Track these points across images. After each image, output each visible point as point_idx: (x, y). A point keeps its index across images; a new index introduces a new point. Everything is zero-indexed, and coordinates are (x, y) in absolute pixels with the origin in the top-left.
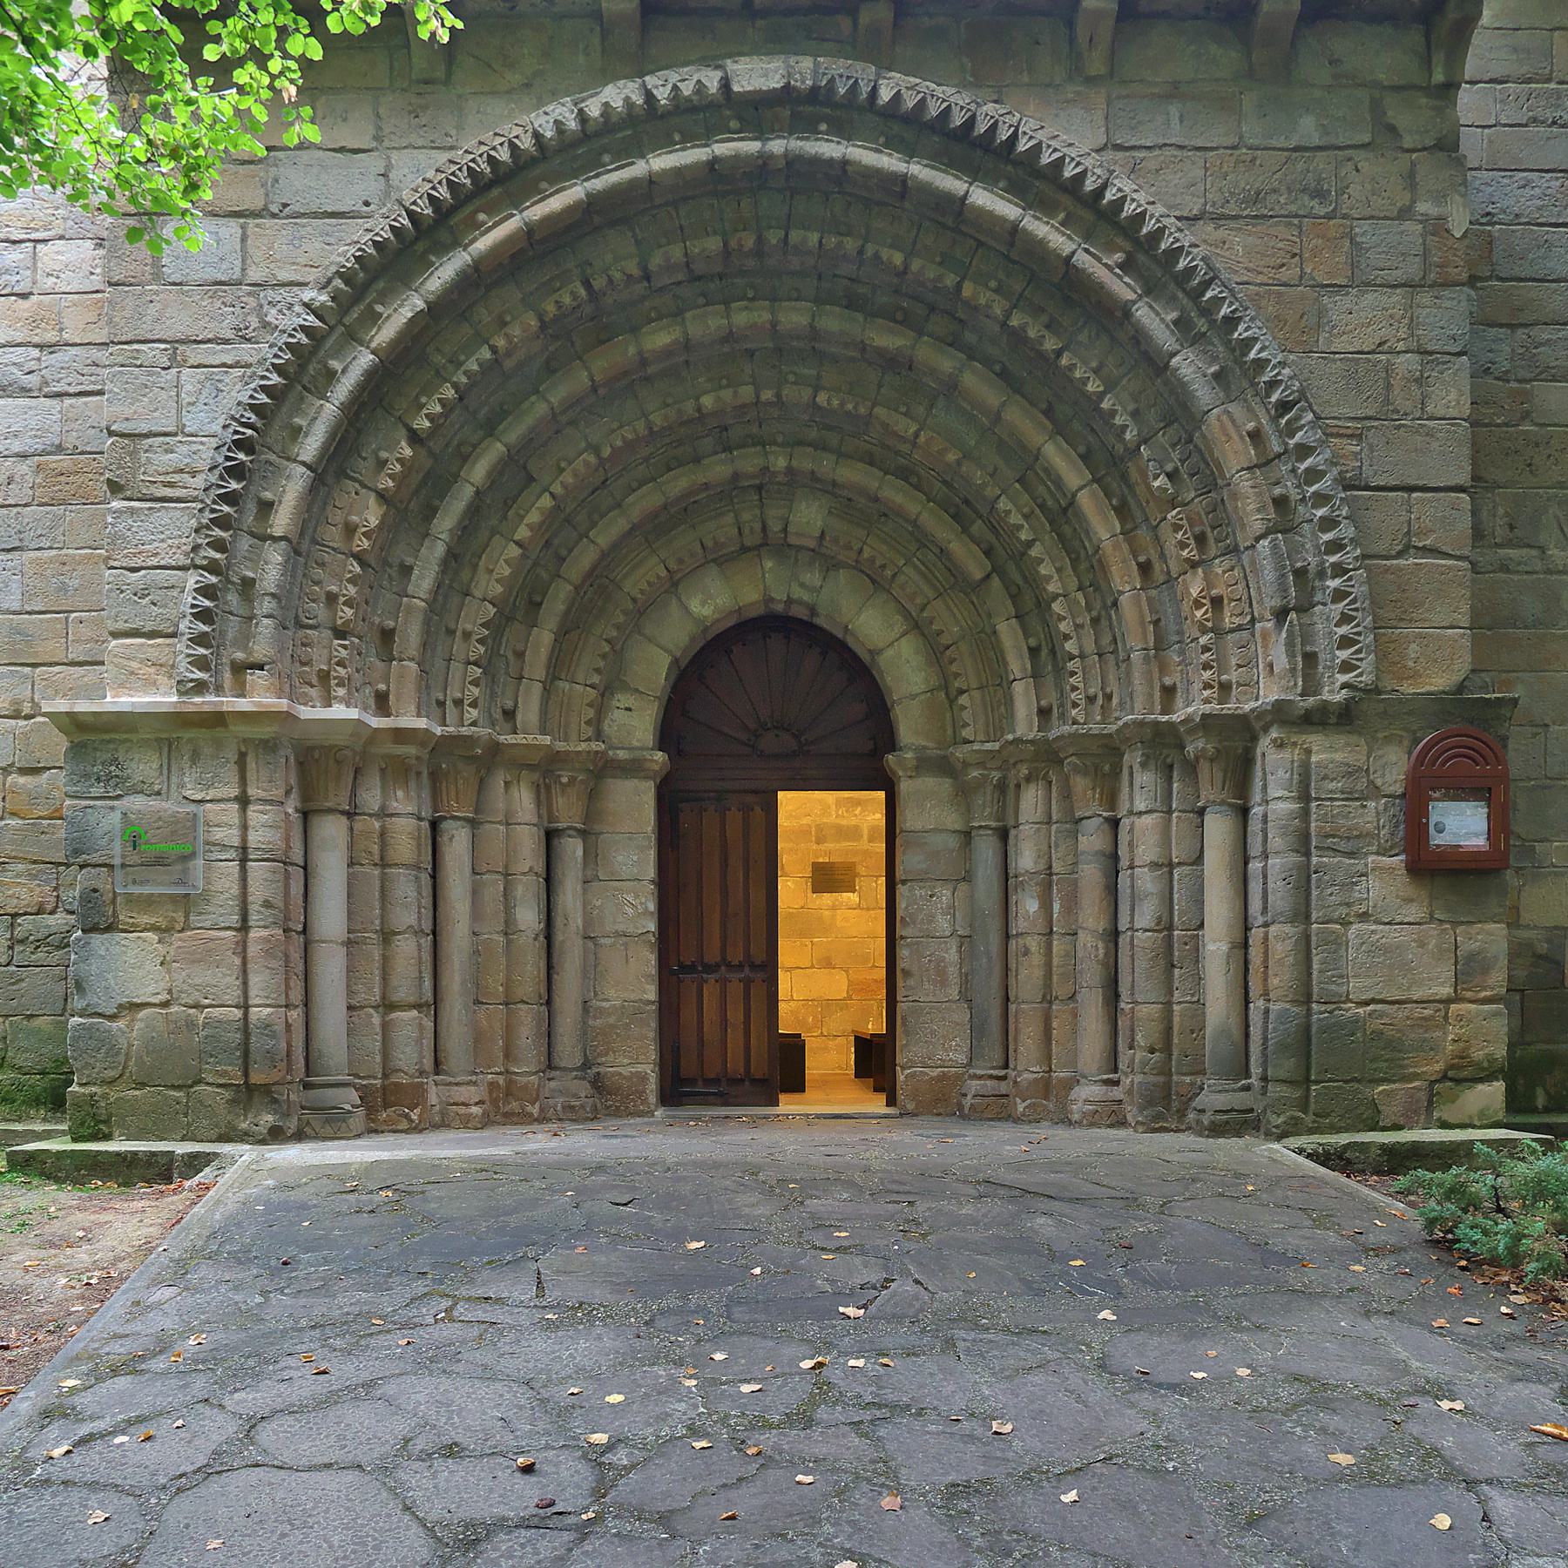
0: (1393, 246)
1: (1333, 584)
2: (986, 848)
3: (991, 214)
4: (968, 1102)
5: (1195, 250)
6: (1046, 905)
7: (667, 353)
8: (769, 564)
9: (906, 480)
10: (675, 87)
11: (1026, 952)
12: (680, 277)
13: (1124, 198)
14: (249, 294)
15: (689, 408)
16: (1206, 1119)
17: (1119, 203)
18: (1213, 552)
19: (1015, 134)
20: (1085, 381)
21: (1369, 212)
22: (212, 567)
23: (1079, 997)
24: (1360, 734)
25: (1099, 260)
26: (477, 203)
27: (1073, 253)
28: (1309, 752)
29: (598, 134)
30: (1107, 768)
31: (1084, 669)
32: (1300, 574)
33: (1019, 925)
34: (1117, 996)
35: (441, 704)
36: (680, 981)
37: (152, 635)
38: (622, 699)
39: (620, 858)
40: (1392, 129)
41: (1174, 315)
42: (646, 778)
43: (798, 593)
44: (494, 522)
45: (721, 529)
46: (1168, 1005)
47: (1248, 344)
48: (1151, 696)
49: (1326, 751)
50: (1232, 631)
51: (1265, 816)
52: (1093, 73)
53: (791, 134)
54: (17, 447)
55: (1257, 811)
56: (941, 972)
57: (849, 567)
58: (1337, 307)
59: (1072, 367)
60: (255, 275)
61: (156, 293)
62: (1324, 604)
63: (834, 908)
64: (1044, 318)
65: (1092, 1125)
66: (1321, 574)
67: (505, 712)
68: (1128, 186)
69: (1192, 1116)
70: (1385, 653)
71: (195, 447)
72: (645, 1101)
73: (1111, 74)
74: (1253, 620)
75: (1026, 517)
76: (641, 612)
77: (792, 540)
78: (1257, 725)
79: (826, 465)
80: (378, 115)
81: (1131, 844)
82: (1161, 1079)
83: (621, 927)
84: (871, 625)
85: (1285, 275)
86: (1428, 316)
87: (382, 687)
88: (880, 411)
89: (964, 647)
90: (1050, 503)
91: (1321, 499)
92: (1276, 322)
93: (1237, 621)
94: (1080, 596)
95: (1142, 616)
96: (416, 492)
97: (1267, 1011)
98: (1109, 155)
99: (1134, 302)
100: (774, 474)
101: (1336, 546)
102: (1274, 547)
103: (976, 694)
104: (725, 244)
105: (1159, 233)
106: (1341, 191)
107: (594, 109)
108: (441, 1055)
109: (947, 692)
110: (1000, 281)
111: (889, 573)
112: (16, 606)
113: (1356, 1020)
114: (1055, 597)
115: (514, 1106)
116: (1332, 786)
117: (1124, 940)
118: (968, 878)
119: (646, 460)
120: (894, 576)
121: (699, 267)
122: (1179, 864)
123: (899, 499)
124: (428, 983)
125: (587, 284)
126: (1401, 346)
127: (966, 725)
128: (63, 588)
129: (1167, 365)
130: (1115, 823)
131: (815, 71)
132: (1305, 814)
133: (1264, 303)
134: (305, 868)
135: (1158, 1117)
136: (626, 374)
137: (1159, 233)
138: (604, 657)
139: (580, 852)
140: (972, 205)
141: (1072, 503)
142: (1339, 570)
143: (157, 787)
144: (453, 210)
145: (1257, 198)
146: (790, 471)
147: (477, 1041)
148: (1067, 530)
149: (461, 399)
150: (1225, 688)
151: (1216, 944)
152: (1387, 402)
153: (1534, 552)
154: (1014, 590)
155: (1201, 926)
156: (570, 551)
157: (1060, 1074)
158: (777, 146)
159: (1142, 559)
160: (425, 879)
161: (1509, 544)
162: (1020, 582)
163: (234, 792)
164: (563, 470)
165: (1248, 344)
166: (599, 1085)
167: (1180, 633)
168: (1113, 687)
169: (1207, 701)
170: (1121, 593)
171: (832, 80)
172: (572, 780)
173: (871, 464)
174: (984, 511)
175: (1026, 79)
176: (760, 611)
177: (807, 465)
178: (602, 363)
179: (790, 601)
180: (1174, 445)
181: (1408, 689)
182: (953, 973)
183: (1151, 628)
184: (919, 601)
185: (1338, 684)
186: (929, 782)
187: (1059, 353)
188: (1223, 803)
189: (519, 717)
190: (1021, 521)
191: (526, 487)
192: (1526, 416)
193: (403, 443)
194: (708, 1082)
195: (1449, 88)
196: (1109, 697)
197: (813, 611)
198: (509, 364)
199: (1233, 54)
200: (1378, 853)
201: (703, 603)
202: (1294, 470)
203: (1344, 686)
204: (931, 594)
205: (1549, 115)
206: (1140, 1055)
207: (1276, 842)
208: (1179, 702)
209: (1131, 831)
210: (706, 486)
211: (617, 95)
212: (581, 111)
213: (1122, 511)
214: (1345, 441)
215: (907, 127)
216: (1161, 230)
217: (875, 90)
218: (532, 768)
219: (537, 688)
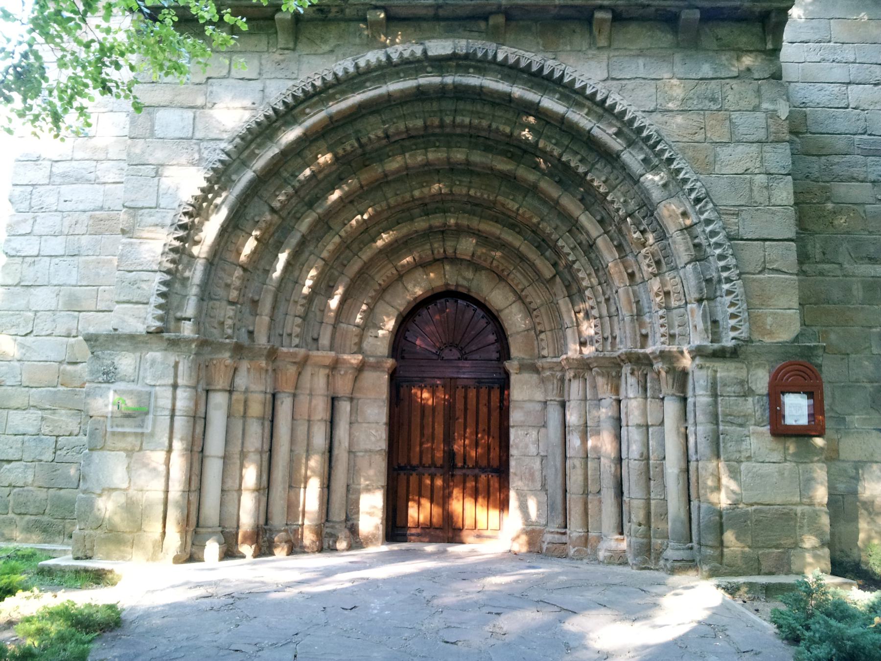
0: (751, 124)
1: (726, 287)
3: (551, 111)
4: (545, 546)
5: (652, 127)
7: (398, 171)
8: (447, 268)
9: (514, 230)
10: (401, 53)
11: (574, 467)
12: (404, 136)
13: (616, 103)
14: (195, 144)
15: (407, 196)
17: (613, 106)
19: (563, 74)
20: (599, 187)
21: (737, 108)
23: (602, 493)
24: (743, 363)
25: (605, 131)
26: (306, 104)
27: (592, 129)
28: (716, 371)
29: (365, 73)
30: (614, 374)
31: (602, 324)
32: (709, 281)
34: (622, 493)
36: (398, 474)
37: (137, 303)
39: (369, 411)
41: (642, 157)
42: (383, 371)
43: (462, 282)
44: (311, 248)
46: (648, 500)
47: (678, 171)
48: (635, 339)
49: (725, 371)
50: (676, 308)
51: (695, 404)
52: (601, 45)
53: (456, 73)
54: (81, 207)
55: (690, 400)
56: (532, 475)
57: (487, 269)
58: (724, 153)
59: (592, 180)
60: (198, 135)
61: (151, 142)
62: (722, 296)
64: (579, 157)
65: (609, 563)
66: (719, 281)
70: (752, 320)
71: (164, 214)
73: (610, 46)
74: (686, 303)
75: (572, 249)
77: (458, 256)
79: (475, 223)
80: (261, 64)
81: (626, 413)
82: (645, 540)
83: (368, 447)
84: (498, 298)
85: (697, 137)
86: (770, 156)
87: (251, 328)
88: (499, 198)
89: (543, 310)
91: (718, 245)
92: (693, 161)
93: (678, 303)
94: (599, 288)
96: (273, 234)
97: (699, 507)
98: (609, 83)
99: (622, 151)
100: (450, 226)
101: (726, 268)
102: (695, 269)
103: (549, 333)
104: (425, 123)
105: (633, 119)
106: (724, 99)
107: (362, 63)
108: (270, 516)
109: (536, 331)
110: (557, 140)
111: (506, 273)
112: (74, 283)
113: (746, 513)
114: (587, 288)
116: (728, 389)
117: (624, 463)
119: (387, 219)
120: (508, 275)
121: (413, 133)
122: (652, 425)
124: (265, 477)
125: (358, 140)
126: (757, 171)
127: (543, 349)
128: (98, 274)
129: (639, 180)
130: (619, 401)
131: (467, 46)
132: (716, 403)
133: (687, 151)
134: (205, 418)
135: (645, 562)
136: (377, 180)
137: (633, 119)
139: (348, 409)
140: (543, 108)
141: (594, 243)
142: (728, 280)
143: (132, 378)
144: (294, 107)
146: (457, 224)
147: (289, 507)
148: (593, 256)
149: (296, 192)
150: (672, 336)
151: (672, 467)
152: (751, 197)
153: (836, 266)
154: (567, 283)
155: (664, 458)
156: (349, 262)
157: (592, 534)
158: (449, 80)
159: (630, 271)
160: (267, 424)
161: (823, 262)
162: (569, 278)
163: (171, 381)
164: (345, 225)
165: (678, 171)
167: (650, 308)
168: (617, 332)
169: (663, 343)
170: (619, 288)
171: (475, 50)
172: (346, 373)
173: (496, 222)
175: (568, 48)
176: (444, 289)
177: (465, 222)
178: (366, 176)
179: (457, 285)
180: (644, 218)
181: (767, 340)
182: (538, 475)
183: (634, 305)
184: (520, 287)
185: (730, 337)
186: (526, 376)
187: (586, 174)
188: (673, 395)
189: (320, 342)
190: (569, 251)
191: (328, 232)
192: (828, 199)
193: (267, 213)
195: (776, 50)
196: (614, 338)
197: (469, 290)
198: (320, 176)
200: (755, 425)
202: (704, 231)
203: (733, 338)
204: (527, 284)
205: (831, 57)
206: (634, 527)
207: (700, 418)
208: (650, 341)
209: (627, 407)
210: (416, 232)
211: (373, 57)
212: (356, 64)
213: (619, 247)
214: (730, 216)
215: (512, 71)
216: (634, 118)
217: (496, 54)
218: (325, 367)
219: (329, 329)
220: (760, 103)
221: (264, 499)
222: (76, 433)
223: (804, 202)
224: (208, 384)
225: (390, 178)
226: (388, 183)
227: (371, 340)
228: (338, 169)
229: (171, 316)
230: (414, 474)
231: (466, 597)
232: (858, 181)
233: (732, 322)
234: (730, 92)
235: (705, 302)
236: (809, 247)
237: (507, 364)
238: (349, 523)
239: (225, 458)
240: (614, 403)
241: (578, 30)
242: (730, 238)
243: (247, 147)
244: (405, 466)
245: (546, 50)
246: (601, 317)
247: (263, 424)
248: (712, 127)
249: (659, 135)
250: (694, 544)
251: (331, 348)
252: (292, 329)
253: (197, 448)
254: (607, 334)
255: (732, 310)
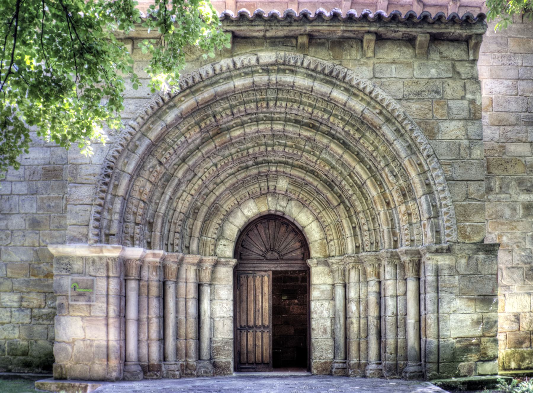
2: (339, 291)
6: (358, 308)
8: (270, 199)
9: (313, 174)
16: (407, 375)
17: (377, 96)
18: (409, 199)
22: (100, 205)
33: (350, 314)
35: (167, 245)
38: (223, 242)
40: (458, 73)
43: (279, 208)
45: (254, 188)
55: (422, 279)
56: (325, 329)
58: (444, 126)
63: (289, 305)
67: (186, 247)
68: (380, 91)
69: (403, 374)
72: (229, 370)
75: (351, 186)
76: (229, 214)
77: (277, 191)
78: (422, 253)
81: (384, 289)
82: (394, 362)
83: (222, 315)
84: (303, 218)
87: (149, 240)
90: (359, 182)
95: (387, 219)
96: (160, 179)
98: (374, 80)
108: (166, 355)
111: (308, 202)
115: (189, 372)
117: (383, 319)
118: (333, 299)
119: (231, 168)
123: (311, 180)
124: (162, 333)
127: (332, 251)
130: (380, 282)
134: (125, 297)
135: (394, 374)
136: (225, 143)
138: (217, 229)
139: (209, 291)
145: (419, 94)
146: (276, 171)
151: (411, 321)
154: (347, 209)
160: (161, 300)
166: (215, 365)
169: (407, 245)
174: (338, 184)
175: (349, 58)
176: (267, 213)
178: (218, 141)
179: (276, 211)
184: (318, 211)
186: (321, 268)
192: (504, 153)
194: (249, 364)
195: (475, 61)
197: (284, 214)
199: (410, 51)
201: (249, 211)
210: (250, 176)
218: (194, 264)
220: (465, 94)
221: (162, 346)
222: (43, 306)
223: (490, 156)
224: (126, 276)
225: (233, 141)
226: (233, 144)
227: (221, 247)
228: (201, 136)
229: (103, 233)
230: (251, 331)
231: (295, 382)
232: (522, 142)
233: (448, 231)
234: (447, 87)
235: (432, 219)
236: (492, 184)
237: (309, 261)
238: (212, 361)
239: (139, 321)
240: (377, 283)
241: (354, 46)
242: (447, 180)
243: (145, 124)
244: (245, 327)
245: (334, 58)
246: (369, 230)
247: (159, 300)
248: (437, 109)
249: (405, 114)
250: (423, 363)
251: (198, 253)
252: (173, 241)
253: (123, 315)
254: (373, 240)
255: (448, 224)
